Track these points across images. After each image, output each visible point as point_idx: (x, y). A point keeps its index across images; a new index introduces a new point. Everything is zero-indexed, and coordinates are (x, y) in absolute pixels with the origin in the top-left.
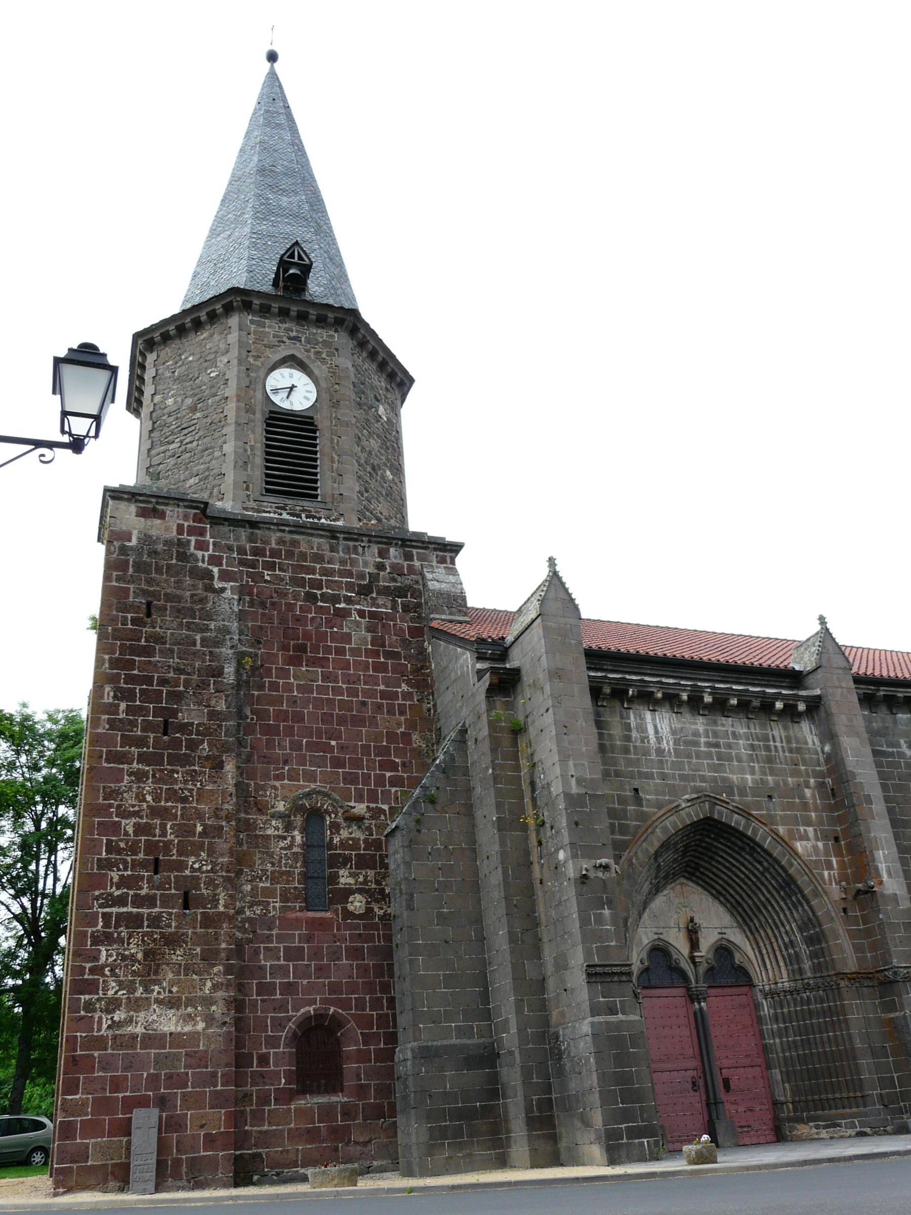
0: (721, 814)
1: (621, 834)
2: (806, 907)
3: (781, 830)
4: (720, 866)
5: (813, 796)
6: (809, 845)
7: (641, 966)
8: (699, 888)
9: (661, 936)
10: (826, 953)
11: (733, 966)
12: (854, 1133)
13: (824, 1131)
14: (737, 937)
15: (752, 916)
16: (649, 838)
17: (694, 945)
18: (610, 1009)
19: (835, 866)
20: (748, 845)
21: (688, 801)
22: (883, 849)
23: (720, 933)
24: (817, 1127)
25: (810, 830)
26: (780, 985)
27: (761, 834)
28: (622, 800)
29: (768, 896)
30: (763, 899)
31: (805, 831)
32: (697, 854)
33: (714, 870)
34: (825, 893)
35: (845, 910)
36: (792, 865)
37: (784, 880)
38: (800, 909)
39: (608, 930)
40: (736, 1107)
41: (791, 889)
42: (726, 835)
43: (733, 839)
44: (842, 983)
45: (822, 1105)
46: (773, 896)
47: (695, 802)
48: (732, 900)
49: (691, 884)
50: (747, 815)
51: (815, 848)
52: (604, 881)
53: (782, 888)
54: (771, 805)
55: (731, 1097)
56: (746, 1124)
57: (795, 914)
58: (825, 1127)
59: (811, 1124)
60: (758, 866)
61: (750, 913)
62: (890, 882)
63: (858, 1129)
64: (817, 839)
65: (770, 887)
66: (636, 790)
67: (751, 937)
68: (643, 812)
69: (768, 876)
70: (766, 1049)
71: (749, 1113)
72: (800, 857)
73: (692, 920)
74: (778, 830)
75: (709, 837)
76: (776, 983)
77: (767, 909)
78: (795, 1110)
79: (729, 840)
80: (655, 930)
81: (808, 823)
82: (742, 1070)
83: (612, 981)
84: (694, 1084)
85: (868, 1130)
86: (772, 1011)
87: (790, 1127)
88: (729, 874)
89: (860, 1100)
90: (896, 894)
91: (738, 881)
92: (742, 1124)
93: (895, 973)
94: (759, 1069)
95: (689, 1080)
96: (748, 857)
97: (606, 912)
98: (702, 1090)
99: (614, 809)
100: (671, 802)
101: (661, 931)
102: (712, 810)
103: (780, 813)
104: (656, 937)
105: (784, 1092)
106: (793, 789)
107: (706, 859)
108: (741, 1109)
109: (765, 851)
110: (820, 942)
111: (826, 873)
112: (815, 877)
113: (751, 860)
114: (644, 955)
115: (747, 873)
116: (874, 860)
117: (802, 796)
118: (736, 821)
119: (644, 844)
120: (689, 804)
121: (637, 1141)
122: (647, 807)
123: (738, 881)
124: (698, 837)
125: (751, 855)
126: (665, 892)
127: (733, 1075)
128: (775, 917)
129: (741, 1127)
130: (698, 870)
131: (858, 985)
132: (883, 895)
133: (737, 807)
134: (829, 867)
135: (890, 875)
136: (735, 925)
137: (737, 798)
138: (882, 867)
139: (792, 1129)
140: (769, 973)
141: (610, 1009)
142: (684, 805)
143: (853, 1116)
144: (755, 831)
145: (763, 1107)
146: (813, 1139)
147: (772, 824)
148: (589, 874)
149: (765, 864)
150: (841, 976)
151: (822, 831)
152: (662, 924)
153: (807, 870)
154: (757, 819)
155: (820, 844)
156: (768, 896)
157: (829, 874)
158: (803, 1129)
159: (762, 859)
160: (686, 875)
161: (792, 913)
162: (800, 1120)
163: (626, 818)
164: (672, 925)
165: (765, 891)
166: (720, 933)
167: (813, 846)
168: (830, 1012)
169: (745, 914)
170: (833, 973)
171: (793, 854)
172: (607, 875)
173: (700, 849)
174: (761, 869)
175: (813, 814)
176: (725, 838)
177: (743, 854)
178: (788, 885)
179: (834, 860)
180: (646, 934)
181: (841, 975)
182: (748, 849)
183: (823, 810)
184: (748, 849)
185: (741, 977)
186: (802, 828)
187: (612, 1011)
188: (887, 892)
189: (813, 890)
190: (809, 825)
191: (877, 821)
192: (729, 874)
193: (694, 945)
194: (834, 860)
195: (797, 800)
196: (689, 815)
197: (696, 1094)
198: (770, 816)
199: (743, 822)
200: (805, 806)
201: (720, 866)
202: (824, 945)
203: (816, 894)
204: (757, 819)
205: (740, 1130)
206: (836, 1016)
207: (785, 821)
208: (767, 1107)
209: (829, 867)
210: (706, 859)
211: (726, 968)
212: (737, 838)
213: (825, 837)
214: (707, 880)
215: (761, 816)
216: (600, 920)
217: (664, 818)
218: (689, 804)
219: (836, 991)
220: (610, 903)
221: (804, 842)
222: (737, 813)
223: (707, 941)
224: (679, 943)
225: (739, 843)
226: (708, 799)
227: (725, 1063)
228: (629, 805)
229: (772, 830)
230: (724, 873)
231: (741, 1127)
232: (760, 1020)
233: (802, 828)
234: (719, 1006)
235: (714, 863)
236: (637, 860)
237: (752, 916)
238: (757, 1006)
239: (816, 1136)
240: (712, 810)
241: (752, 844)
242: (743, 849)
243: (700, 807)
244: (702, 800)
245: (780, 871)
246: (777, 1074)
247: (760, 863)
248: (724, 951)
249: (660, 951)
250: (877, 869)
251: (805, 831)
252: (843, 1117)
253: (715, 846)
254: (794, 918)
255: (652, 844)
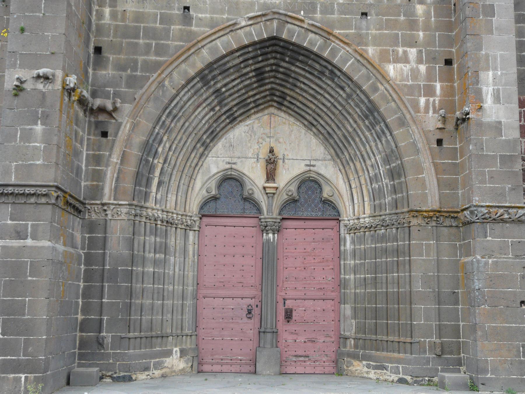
0: (292, 33)
1: (157, 54)
2: (389, 137)
3: (371, 51)
4: (304, 94)
5: (427, 14)
6: (406, 68)
7: (206, 194)
8: (292, 119)
9: (234, 166)
10: (404, 189)
11: (242, 195)
12: (396, 379)
13: (373, 371)
14: (328, 170)
15: (343, 148)
16: (191, 59)
17: (271, 176)
18: (18, 233)
19: (438, 91)
20: (326, 67)
21: (250, 19)
22: (495, 69)
23: (307, 165)
24: (368, 366)
25: (413, 52)
26: (362, 221)
27: (342, 57)
28: (166, 19)
29: (355, 126)
30: (350, 129)
31: (405, 52)
32: (278, 81)
33: (300, 98)
34: (414, 121)
35: (440, 142)
36: (376, 89)
37: (367, 107)
38: (384, 139)
39: (36, 148)
40: (295, 337)
41: (374, 118)
42: (301, 58)
43: (310, 62)
44: (414, 222)
45: (377, 346)
46: (358, 126)
47: (259, 20)
48: (323, 131)
49: (282, 114)
50: (327, 34)
51: (415, 73)
52: (44, 94)
53: (367, 117)
54: (364, 23)
55: (291, 327)
56: (304, 354)
57: (380, 146)
58: (376, 368)
59: (364, 363)
60: (341, 92)
61: (341, 145)
62: (495, 107)
63: (401, 376)
64: (420, 61)
65: (355, 116)
66: (187, 8)
67: (343, 171)
68: (191, 32)
69: (352, 103)
70: (342, 284)
71: (309, 344)
72: (388, 82)
73: (271, 151)
74: (366, 51)
75: (284, 61)
76: (358, 219)
77: (354, 141)
78: (356, 346)
79: (306, 64)
80: (228, 160)
81: (412, 43)
82: (311, 302)
83: (25, 203)
84: (249, 312)
85: (408, 378)
86: (352, 247)
87: (348, 362)
88: (316, 102)
89: (408, 345)
90: (500, 123)
91: (325, 110)
92: (298, 353)
93: (472, 213)
94: (332, 302)
95: (245, 307)
96: (329, 82)
97: (39, 128)
98: (257, 319)
99: (154, 29)
100: (228, 20)
101: (235, 160)
102: (280, 29)
103: (374, 32)
104: (228, 166)
105: (350, 328)
106: (400, 5)
107: (289, 86)
108: (301, 339)
109: (344, 74)
110: (399, 176)
111: (422, 101)
112: (404, 104)
113: (333, 85)
114: (213, 185)
115: (332, 101)
116: (477, 82)
117: (410, 14)
118: (312, 42)
119: (183, 66)
120: (250, 22)
121: (12, 376)
122: (197, 26)
123: (325, 110)
124: (272, 61)
125: (333, 80)
126: (248, 122)
127: (298, 306)
128: (362, 149)
129: (296, 356)
130: (284, 99)
131: (434, 224)
132: (480, 124)
133: (313, 25)
134: (429, 91)
135: (497, 99)
136: (329, 157)
137: (318, 16)
138: (488, 92)
139: (350, 364)
140: (355, 206)
141: (18, 233)
142: (243, 23)
143: (399, 361)
144: (334, 52)
145: (328, 339)
146: (363, 377)
147: (359, 44)
148: (25, 86)
149: (348, 90)
150: (412, 214)
151: (428, 53)
152: (237, 154)
153: (395, 96)
154: (337, 38)
155: (423, 68)
156: (355, 126)
157: (427, 102)
158: (359, 367)
159: (343, 84)
160: (275, 104)
161: (376, 145)
162: (355, 357)
163: (168, 38)
164: (250, 155)
165: (351, 121)
166: (307, 165)
167: (412, 70)
168: (397, 252)
169: (339, 147)
170: (406, 210)
171: (380, 77)
172: (50, 87)
173: (280, 76)
174: (344, 95)
175: (421, 34)
176: (301, 62)
177: (324, 79)
178: (372, 113)
179: (438, 86)
180: (217, 163)
181: (416, 213)
182: (327, 73)
183: (437, 29)
184: (327, 73)
185: (330, 210)
186: (400, 50)
187: (20, 235)
188: (486, 119)
189: (399, 118)
190: (411, 46)
191: (495, 36)
192: (316, 102)
193: (271, 176)
194: (438, 86)
195: (402, 18)
196: (247, 34)
197: (249, 321)
198: (360, 36)
199: (320, 41)
200: (412, 24)
201: (304, 94)
202: (403, 179)
203: (402, 122)
204: (337, 38)
205: (294, 359)
206: (402, 256)
207: (377, 41)
208: (333, 340)
209: (429, 91)
210: (289, 86)
211: (310, 200)
212: (314, 61)
213: (432, 59)
214: (296, 109)
215: (347, 35)
216: (28, 136)
217: (213, 37)
218: (250, 22)
219: (407, 230)
220: (46, 118)
221: (399, 65)
222: (312, 32)
223: (287, 174)
224: (254, 174)
225: (317, 66)
226: (276, 16)
227: (291, 294)
228: (173, 24)
229: (356, 51)
230: (311, 102)
231: (296, 356)
232: (340, 255)
233: (400, 50)
234: (298, 239)
235: (298, 90)
236: (170, 82)
237: (343, 148)
238: (341, 241)
239: (365, 375)
240: (280, 29)
241: (330, 67)
242: (322, 73)
243: (265, 26)
244: (269, 17)
245: (363, 97)
246: (347, 309)
247: (342, 88)
248: (310, 183)
249: (231, 180)
250: (479, 93)
251: (405, 52)
252: (391, 360)
253: (295, 72)
254: (378, 148)
255: (193, 65)
